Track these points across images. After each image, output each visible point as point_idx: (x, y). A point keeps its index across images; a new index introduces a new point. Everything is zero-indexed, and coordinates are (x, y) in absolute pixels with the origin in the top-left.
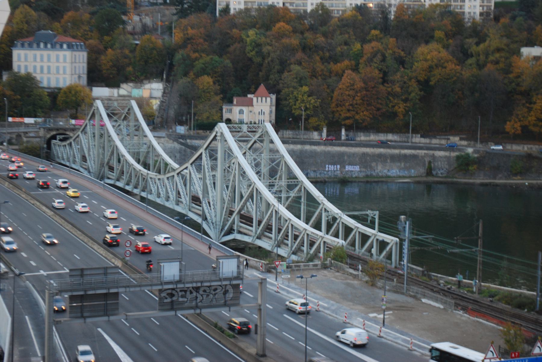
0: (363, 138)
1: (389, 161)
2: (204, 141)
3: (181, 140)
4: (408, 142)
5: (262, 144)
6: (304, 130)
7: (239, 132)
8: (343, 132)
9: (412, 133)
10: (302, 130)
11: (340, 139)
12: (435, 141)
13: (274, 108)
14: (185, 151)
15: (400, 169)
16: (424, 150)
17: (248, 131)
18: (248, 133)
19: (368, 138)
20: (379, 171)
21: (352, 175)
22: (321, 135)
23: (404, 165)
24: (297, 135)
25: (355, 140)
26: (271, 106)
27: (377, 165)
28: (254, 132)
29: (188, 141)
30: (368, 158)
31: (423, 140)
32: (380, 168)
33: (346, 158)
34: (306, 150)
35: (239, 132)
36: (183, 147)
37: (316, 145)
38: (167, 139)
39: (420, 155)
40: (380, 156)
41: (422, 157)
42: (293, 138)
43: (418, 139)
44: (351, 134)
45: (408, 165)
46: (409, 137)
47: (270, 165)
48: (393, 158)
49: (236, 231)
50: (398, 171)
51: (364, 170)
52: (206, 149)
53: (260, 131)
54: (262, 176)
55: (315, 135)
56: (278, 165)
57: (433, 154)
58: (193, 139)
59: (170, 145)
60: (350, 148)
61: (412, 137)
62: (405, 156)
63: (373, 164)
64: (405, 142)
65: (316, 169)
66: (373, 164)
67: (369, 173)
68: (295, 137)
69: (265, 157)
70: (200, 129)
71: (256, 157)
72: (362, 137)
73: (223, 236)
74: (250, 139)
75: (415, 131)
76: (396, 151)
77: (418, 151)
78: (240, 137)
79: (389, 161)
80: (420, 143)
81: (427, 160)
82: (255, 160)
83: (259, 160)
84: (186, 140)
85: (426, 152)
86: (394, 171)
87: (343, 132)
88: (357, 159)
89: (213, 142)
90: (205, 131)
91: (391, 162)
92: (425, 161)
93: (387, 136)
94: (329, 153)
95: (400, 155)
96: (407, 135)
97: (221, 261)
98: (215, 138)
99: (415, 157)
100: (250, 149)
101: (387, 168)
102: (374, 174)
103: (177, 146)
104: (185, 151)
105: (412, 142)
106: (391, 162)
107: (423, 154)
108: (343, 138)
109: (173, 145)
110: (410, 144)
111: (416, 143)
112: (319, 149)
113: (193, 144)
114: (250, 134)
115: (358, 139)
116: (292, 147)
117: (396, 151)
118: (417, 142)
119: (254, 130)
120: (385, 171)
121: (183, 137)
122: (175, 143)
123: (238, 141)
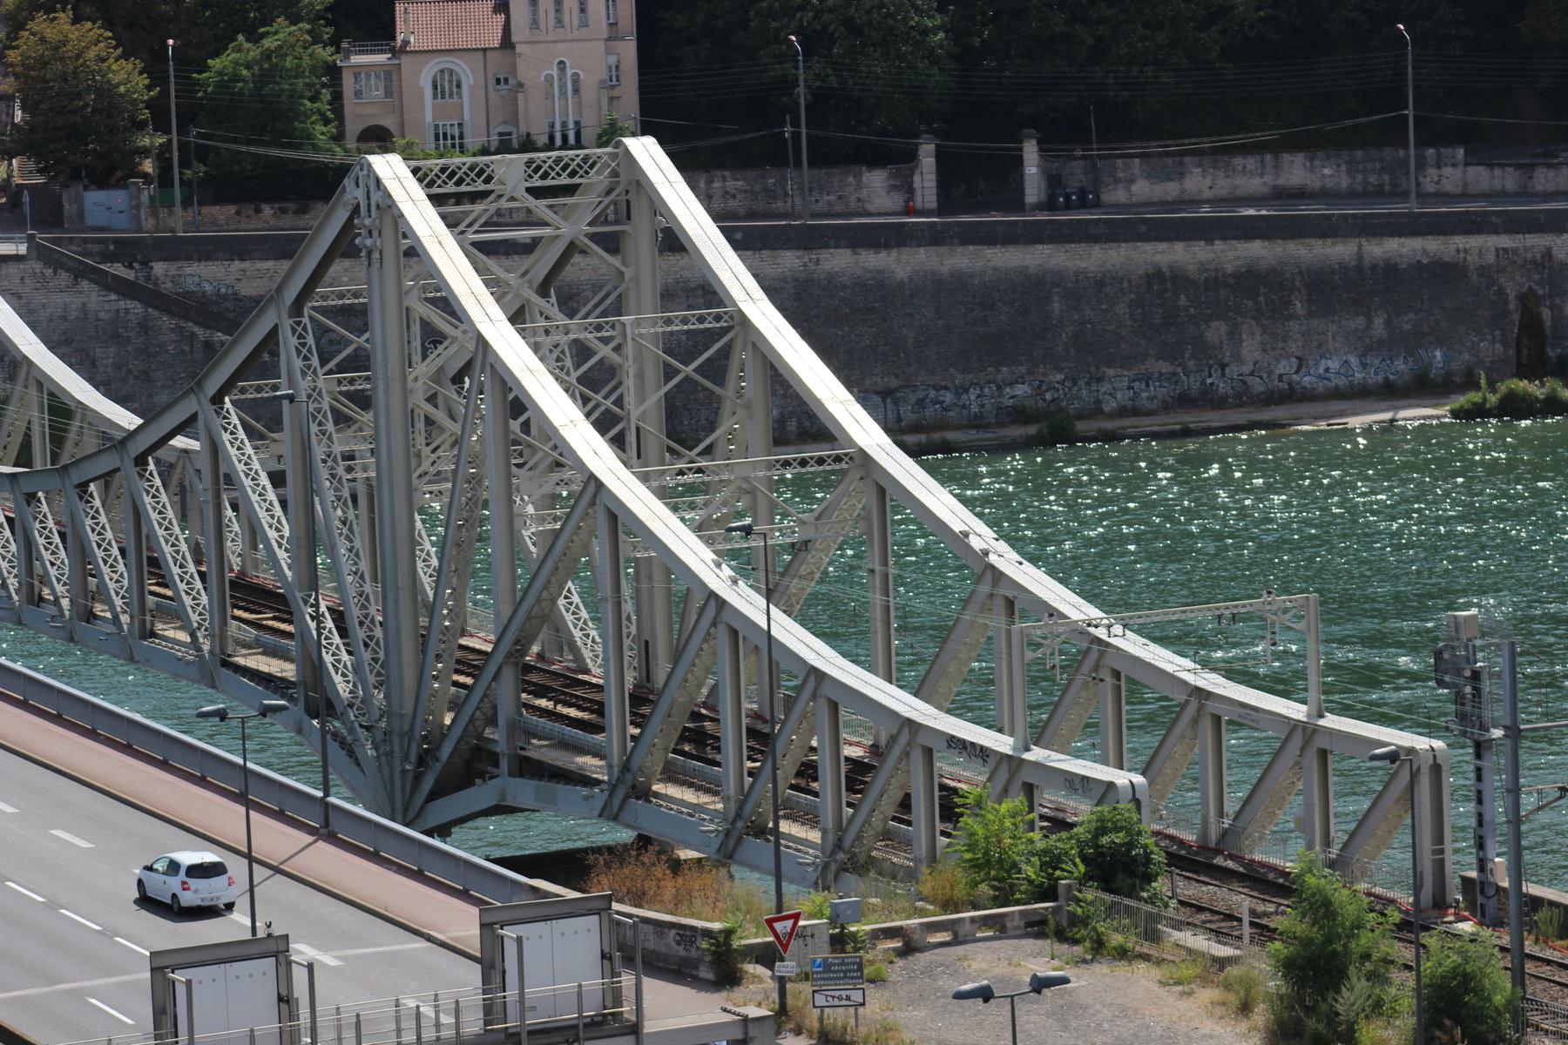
0: (1143, 189)
1: (1299, 307)
2: (286, 265)
3: (118, 269)
4: (1405, 195)
5: (615, 261)
6: (811, 164)
7: (483, 195)
8: (1031, 154)
9: (1422, 143)
10: (798, 164)
11: (1018, 204)
12: (1199, 181)
13: (628, 50)
14: (145, 327)
15: (1368, 350)
16: (1496, 232)
17: (536, 192)
18: (531, 202)
19: (1171, 190)
20: (1246, 369)
21: (1098, 402)
22: (910, 191)
23: (1388, 323)
24: (771, 195)
25: (1098, 204)
26: (613, 36)
27: (1234, 335)
28: (570, 190)
29: (159, 268)
30: (1183, 301)
31: (1481, 177)
32: (1251, 348)
33: (1056, 306)
34: (832, 277)
35: (475, 197)
36: (135, 307)
37: (887, 246)
38: (38, 266)
39: (1473, 260)
40: (1250, 280)
41: (1483, 270)
42: (752, 215)
43: (1454, 175)
44: (1076, 174)
45: (1407, 322)
46: (1404, 163)
47: (670, 372)
48: (1330, 291)
49: (504, 764)
50: (1353, 360)
51: (1164, 367)
52: (297, 308)
53: (597, 179)
54: (631, 438)
55: (875, 189)
56: (717, 370)
57: (1548, 253)
58: (189, 258)
59: (58, 299)
60: (1082, 248)
61: (1421, 164)
62: (1390, 271)
63: (1215, 332)
64: (1379, 194)
65: (894, 383)
66: (1215, 332)
67: (1192, 384)
68: (761, 206)
69: (645, 324)
70: (218, 199)
71: (590, 337)
72: (1136, 186)
73: (433, 796)
74: (546, 231)
75: (1434, 135)
76: (1340, 251)
77: (1461, 241)
78: (489, 225)
79: (1299, 307)
80: (1465, 196)
81: (1512, 287)
82: (582, 352)
83: (604, 351)
84: (145, 263)
85: (1505, 241)
86: (1334, 365)
87: (1031, 154)
88: (1122, 309)
89: (338, 267)
90: (249, 209)
91: (1311, 315)
92: (1501, 292)
93: (1277, 167)
94: (959, 283)
95: (1359, 268)
96: (1388, 153)
97: (509, 932)
98: (345, 247)
99: (1443, 273)
100: (543, 290)
101: (1294, 347)
102: (1223, 387)
103: (91, 297)
104: (145, 327)
105: (1423, 196)
106: (1311, 315)
107: (1491, 258)
108: (1033, 190)
109: (74, 301)
110: (1412, 206)
111: (1442, 197)
112: (899, 264)
113: (190, 285)
114: (540, 206)
115: (1119, 195)
116: (789, 261)
117: (1340, 251)
118: (1448, 187)
119: (564, 180)
120: (1284, 367)
121: (126, 250)
122: (85, 285)
123: (483, 252)
